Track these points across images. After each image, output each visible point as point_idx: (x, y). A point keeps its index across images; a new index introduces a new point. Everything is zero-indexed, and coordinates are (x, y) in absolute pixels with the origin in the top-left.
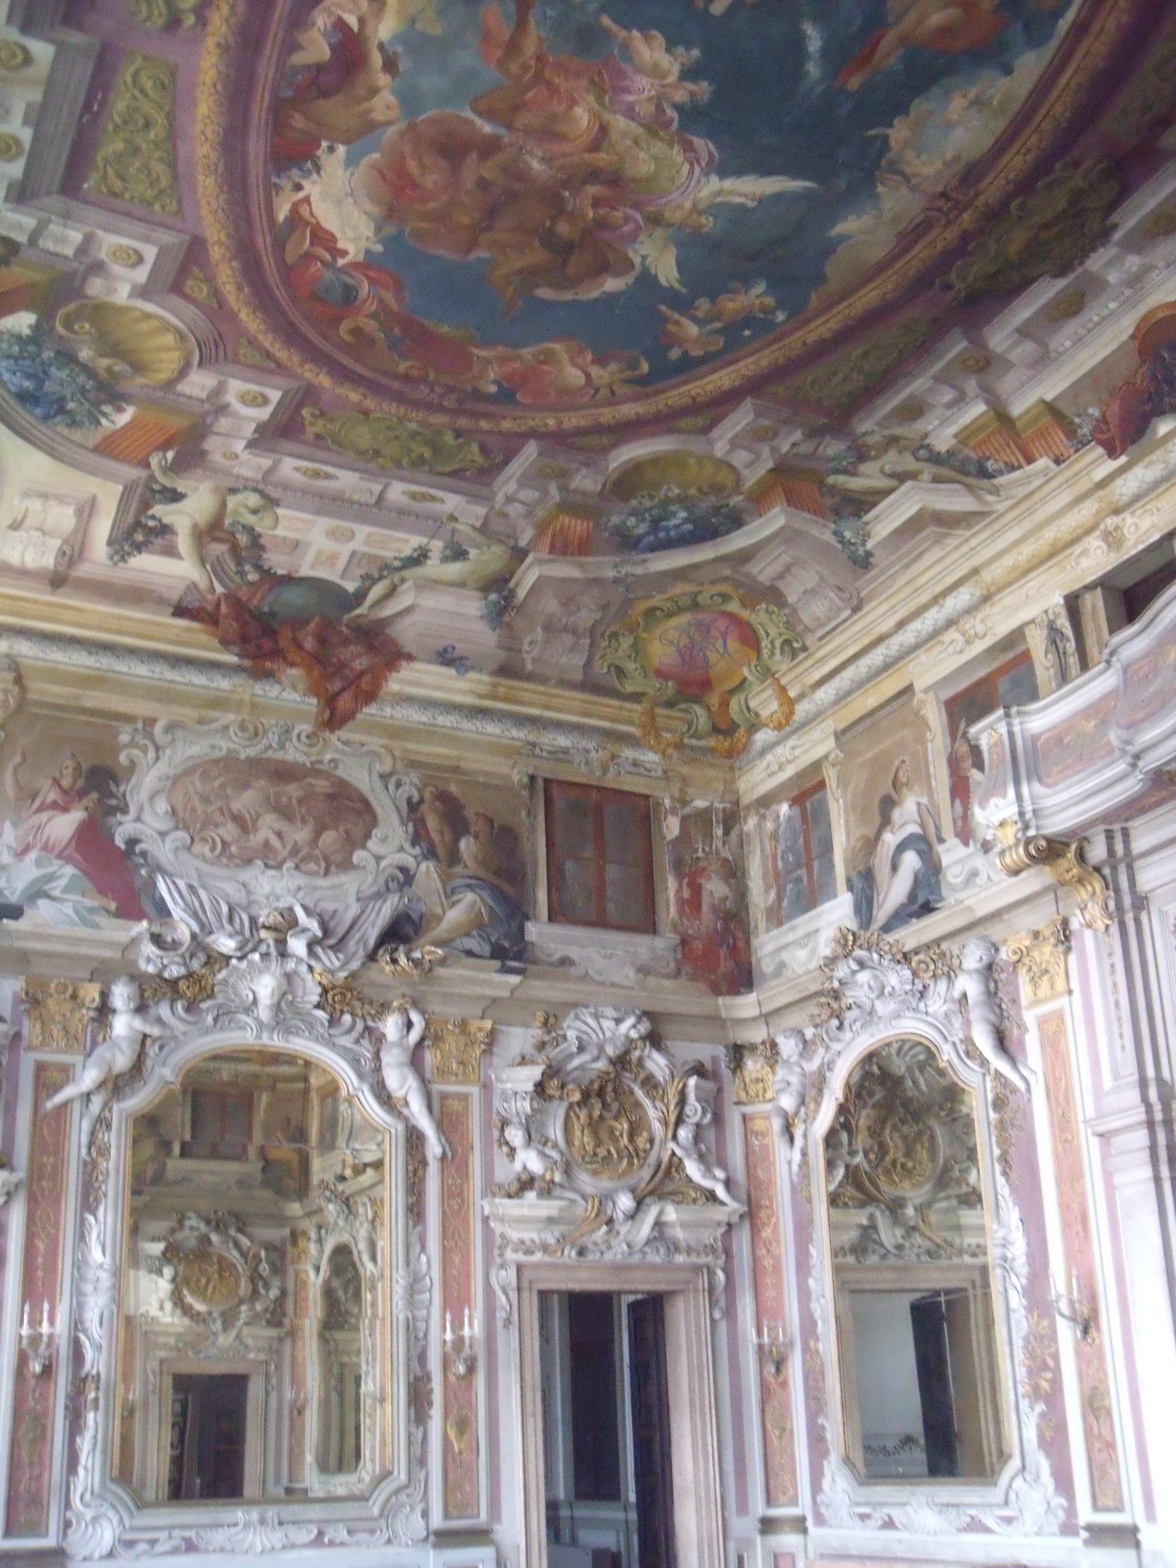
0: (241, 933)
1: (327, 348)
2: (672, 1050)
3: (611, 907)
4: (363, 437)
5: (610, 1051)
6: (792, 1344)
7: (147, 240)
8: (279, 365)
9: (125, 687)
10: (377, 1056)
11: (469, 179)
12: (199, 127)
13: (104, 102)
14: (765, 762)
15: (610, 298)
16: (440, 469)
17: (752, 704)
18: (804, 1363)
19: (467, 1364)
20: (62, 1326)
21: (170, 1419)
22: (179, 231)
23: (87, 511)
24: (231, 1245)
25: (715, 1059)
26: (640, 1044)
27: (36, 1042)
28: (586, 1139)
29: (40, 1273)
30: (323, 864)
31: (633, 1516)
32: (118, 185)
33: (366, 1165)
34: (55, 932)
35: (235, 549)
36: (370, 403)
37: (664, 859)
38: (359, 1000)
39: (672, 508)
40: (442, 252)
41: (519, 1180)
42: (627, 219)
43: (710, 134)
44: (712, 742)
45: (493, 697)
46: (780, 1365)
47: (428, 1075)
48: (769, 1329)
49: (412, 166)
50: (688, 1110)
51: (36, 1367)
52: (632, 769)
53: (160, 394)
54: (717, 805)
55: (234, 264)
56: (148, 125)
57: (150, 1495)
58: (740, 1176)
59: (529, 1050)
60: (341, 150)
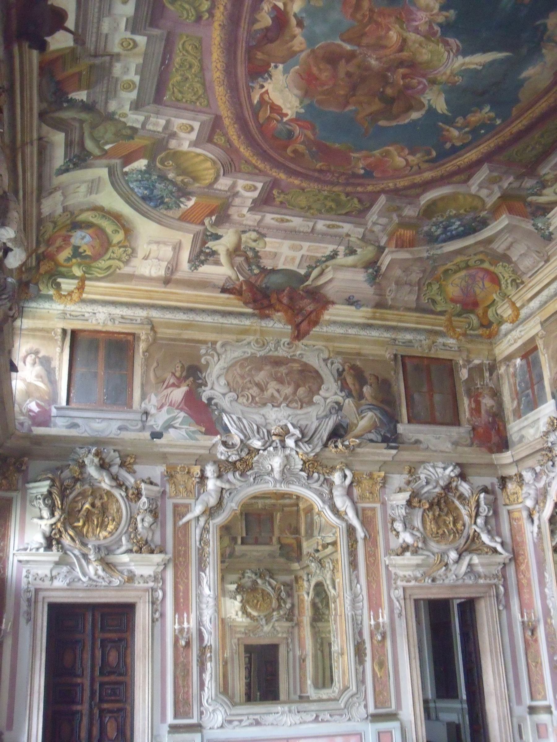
0: (264, 438)
1: (281, 160)
2: (472, 481)
3: (437, 414)
4: (302, 201)
5: (442, 483)
6: (539, 621)
7: (194, 119)
8: (260, 171)
9: (201, 328)
10: (331, 493)
11: (342, 73)
12: (214, 64)
13: (171, 59)
14: (508, 339)
15: (414, 123)
16: (339, 212)
17: (499, 312)
18: (545, 629)
19: (382, 635)
20: (193, 624)
21: (244, 666)
22: (209, 114)
23: (177, 248)
24: (267, 584)
25: (492, 484)
26: (456, 479)
27: (173, 494)
28: (432, 526)
29: (182, 600)
30: (299, 404)
31: (465, 706)
32: (180, 96)
33: (328, 544)
34: (178, 443)
35: (247, 259)
36: (304, 185)
37: (461, 390)
38: (320, 466)
39: (453, 220)
40: (332, 109)
41: (402, 547)
42: (419, 83)
43: (457, 36)
44: (480, 332)
45: (374, 318)
46: (533, 631)
47: (356, 500)
48: (527, 613)
49: (315, 70)
50: (481, 510)
51: (183, 643)
52: (443, 348)
53: (206, 190)
54: (485, 362)
55: (236, 126)
56: (191, 67)
57: (237, 699)
58: (508, 540)
59: (403, 485)
60: (281, 66)
